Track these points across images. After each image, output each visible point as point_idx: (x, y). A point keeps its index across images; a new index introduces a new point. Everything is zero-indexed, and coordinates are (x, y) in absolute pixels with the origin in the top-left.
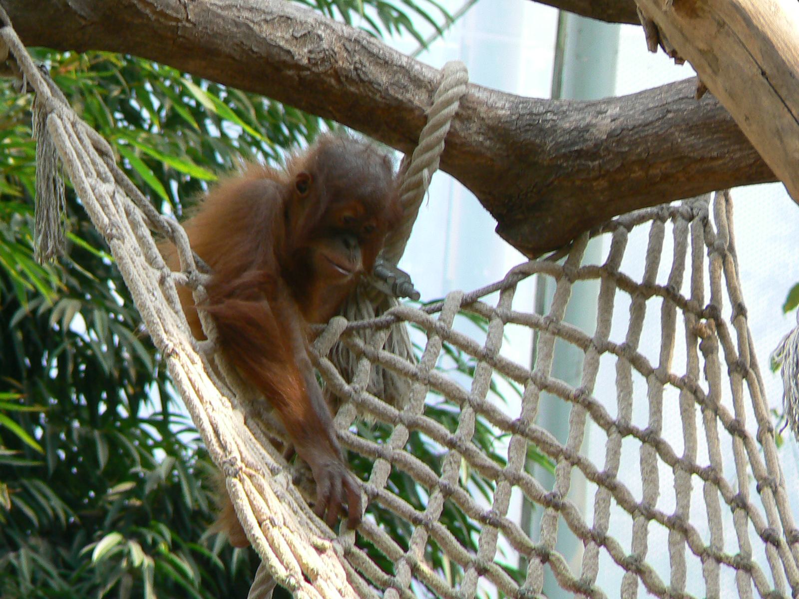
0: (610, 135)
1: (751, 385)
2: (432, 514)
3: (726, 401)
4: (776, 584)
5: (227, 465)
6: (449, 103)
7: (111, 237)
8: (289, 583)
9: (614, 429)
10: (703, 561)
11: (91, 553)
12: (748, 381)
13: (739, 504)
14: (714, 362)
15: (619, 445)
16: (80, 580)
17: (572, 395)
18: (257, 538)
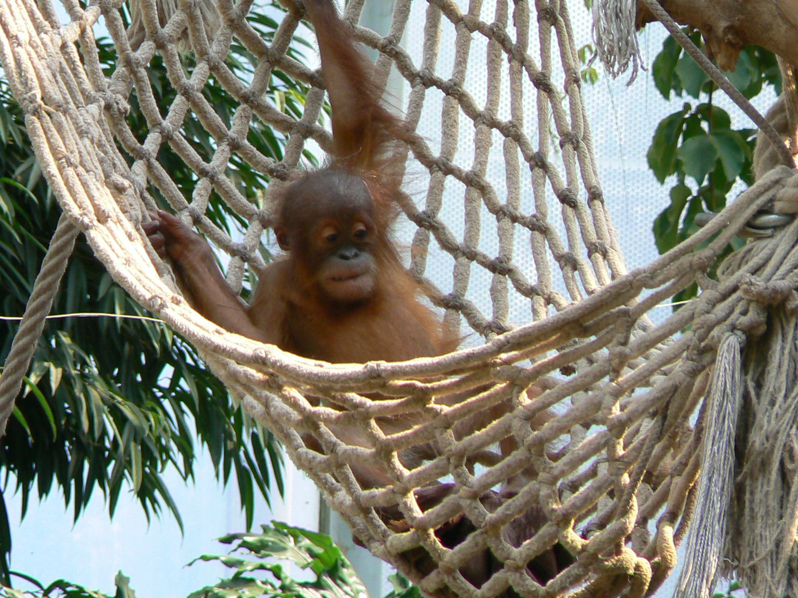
1: (559, 33)
2: (218, 167)
3: (533, 51)
4: (571, 246)
5: (27, 102)
8: (82, 221)
9: (418, 80)
10: (498, 220)
12: (556, 28)
13: (538, 162)
14: (523, 10)
15: (422, 97)
17: (379, 45)
18: (53, 175)
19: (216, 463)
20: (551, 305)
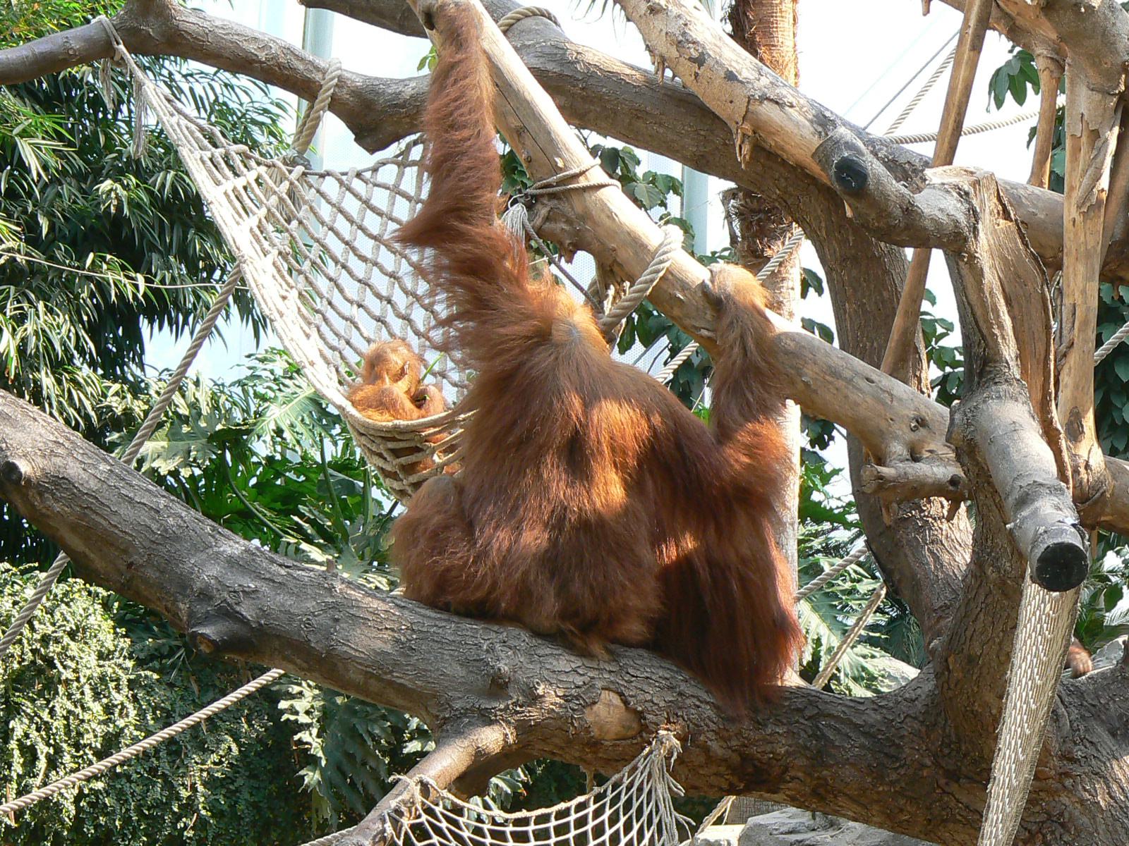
0: (411, 97)
6: (332, 79)
7: (178, 145)
11: (98, 189)
16: (93, 200)
19: (242, 320)
20: (553, 265)
